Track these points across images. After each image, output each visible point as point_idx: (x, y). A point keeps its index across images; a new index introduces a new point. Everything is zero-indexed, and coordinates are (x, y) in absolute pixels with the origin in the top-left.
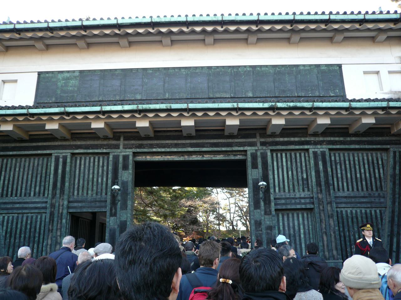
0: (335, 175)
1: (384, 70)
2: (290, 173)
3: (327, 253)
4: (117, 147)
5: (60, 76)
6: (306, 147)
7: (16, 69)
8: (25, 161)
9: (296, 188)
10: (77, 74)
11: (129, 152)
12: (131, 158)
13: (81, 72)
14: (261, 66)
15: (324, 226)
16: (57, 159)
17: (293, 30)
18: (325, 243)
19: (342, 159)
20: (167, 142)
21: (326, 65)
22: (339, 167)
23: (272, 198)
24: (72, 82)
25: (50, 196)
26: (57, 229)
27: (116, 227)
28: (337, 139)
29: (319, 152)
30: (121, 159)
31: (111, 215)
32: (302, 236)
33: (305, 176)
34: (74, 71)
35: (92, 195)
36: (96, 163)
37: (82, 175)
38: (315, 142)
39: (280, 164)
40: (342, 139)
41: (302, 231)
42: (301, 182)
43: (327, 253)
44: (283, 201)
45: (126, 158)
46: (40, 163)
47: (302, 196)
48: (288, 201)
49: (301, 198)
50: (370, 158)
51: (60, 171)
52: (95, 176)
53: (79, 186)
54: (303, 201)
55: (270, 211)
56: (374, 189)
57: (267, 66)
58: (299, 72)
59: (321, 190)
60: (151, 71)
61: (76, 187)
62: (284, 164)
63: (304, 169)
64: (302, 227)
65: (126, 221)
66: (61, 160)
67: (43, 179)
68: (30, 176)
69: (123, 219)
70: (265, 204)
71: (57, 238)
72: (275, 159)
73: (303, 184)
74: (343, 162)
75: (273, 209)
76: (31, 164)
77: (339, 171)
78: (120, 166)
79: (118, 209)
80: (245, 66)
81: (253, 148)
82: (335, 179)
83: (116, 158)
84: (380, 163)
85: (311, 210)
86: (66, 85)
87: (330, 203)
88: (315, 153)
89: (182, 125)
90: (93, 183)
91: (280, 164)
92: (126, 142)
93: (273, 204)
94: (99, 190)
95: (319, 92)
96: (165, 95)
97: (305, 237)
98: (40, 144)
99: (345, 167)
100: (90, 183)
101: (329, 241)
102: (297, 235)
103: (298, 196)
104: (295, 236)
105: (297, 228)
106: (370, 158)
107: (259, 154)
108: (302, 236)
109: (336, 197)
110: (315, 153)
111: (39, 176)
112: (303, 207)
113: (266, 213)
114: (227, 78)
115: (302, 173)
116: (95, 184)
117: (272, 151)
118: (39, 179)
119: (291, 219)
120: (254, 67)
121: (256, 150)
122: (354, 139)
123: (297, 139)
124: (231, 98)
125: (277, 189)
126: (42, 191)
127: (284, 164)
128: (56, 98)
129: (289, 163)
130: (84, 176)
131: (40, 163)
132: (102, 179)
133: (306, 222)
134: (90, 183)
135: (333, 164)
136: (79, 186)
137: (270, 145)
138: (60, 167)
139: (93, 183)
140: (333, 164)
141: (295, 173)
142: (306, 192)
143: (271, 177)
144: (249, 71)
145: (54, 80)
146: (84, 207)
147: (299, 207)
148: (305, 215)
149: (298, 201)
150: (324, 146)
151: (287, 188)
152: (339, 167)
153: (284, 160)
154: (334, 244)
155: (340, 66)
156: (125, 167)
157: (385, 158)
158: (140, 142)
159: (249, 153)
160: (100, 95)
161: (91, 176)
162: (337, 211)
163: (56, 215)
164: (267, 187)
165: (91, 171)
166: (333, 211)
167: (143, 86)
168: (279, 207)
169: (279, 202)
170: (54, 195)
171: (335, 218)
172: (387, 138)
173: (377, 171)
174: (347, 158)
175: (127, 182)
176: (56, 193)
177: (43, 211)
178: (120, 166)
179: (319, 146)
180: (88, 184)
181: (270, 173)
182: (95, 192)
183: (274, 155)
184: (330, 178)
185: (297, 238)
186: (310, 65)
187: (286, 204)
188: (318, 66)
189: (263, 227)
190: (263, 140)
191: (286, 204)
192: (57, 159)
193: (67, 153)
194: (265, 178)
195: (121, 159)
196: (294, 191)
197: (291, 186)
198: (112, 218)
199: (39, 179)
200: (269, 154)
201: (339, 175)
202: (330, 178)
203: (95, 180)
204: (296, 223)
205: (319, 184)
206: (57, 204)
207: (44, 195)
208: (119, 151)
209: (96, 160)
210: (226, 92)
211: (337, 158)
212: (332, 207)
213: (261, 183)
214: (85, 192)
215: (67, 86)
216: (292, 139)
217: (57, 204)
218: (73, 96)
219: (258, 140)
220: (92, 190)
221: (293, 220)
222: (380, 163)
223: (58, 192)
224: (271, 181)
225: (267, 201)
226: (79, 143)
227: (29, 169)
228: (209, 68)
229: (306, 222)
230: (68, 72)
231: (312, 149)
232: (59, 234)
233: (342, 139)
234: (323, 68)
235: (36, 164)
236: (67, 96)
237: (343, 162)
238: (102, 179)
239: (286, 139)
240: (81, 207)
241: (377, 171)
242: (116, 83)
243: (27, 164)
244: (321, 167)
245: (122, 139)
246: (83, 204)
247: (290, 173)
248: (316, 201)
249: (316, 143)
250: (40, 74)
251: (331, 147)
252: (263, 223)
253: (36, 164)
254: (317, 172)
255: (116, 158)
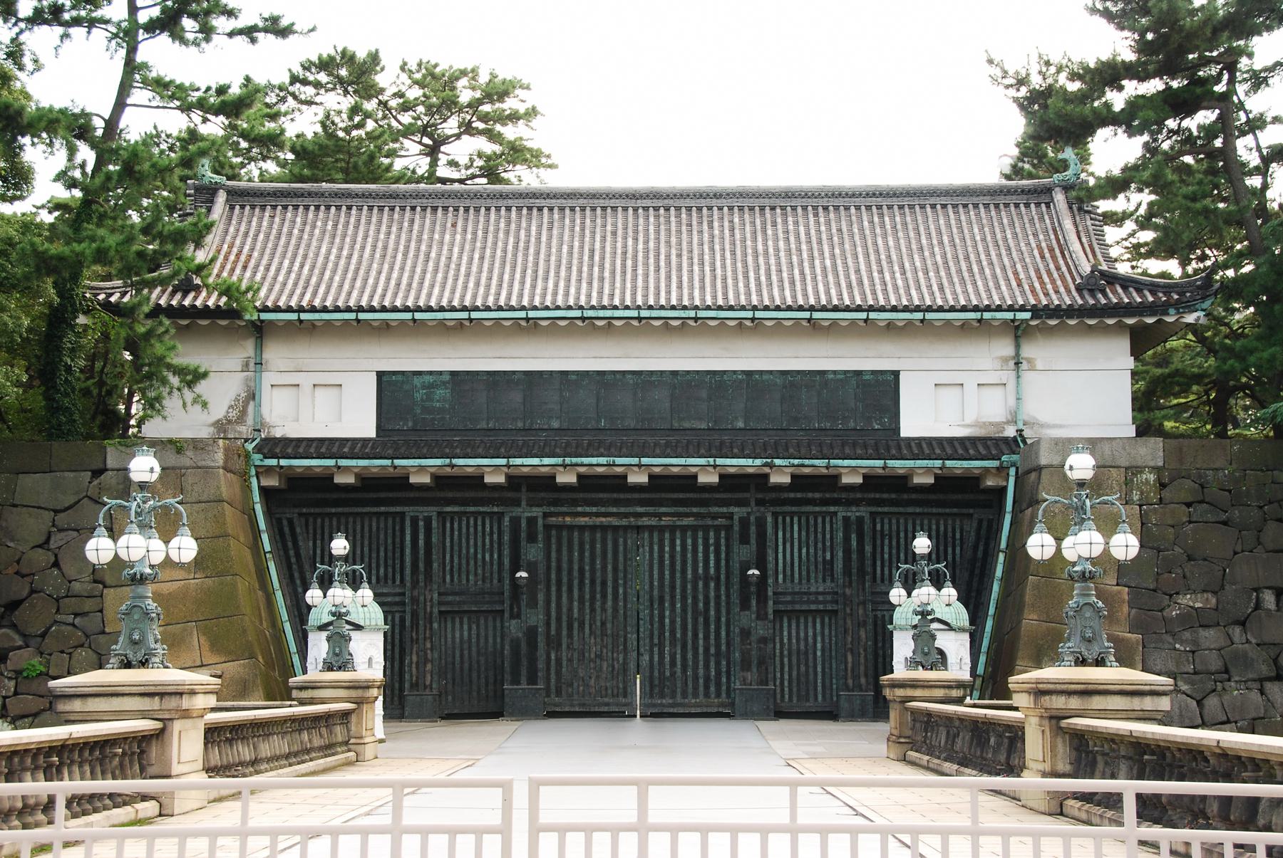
0: (878, 556)
1: (970, 381)
2: (804, 550)
3: (850, 682)
4: (517, 503)
5: (417, 381)
6: (832, 509)
7: (337, 364)
8: (354, 522)
9: (813, 575)
10: (447, 378)
11: (537, 512)
12: (540, 522)
13: (453, 373)
14: (761, 372)
15: (849, 639)
16: (414, 521)
17: (813, 323)
18: (850, 665)
19: (894, 527)
20: (601, 495)
21: (873, 372)
22: (886, 542)
23: (770, 593)
24: (440, 392)
25: (408, 584)
26: (425, 639)
27: (520, 635)
28: (885, 496)
29: (853, 518)
30: (524, 524)
31: (512, 617)
32: (819, 653)
33: (828, 557)
34: (441, 373)
35: (476, 582)
36: (480, 528)
37: (456, 548)
38: (847, 500)
39: (788, 535)
40: (893, 496)
41: (819, 646)
42: (820, 567)
43: (850, 682)
44: (789, 598)
45: (532, 521)
46: (382, 525)
47: (821, 589)
48: (797, 598)
49: (818, 593)
50: (942, 528)
51: (421, 542)
52: (480, 551)
53: (452, 567)
54: (821, 598)
55: (766, 614)
56: (796, 581)
57: (771, 372)
58: (826, 384)
59: (850, 582)
60: (574, 377)
61: (448, 568)
62: (796, 535)
63: (828, 544)
64: (819, 639)
65: (536, 627)
66: (421, 523)
67: (390, 554)
68: (366, 549)
69: (532, 622)
70: (758, 602)
71: (426, 654)
72: (780, 526)
73: (824, 569)
74: (894, 534)
75: (770, 611)
76: (366, 529)
77: (886, 549)
78: (523, 535)
79: (523, 608)
80: (735, 372)
81: (744, 510)
82: (879, 563)
83: (515, 522)
84: (958, 536)
85: (835, 612)
86: (429, 397)
87: (864, 603)
88: (846, 519)
89: (373, 434)
90: (476, 563)
91: (788, 535)
92: (532, 495)
93: (771, 603)
94: (488, 575)
95: (855, 421)
96: (599, 421)
97: (823, 655)
98: (383, 495)
99: (898, 542)
100: (472, 562)
101: (856, 664)
102: (811, 651)
103: (813, 589)
104: (806, 653)
105: (810, 640)
106: (942, 528)
107: (752, 518)
108: (819, 653)
109: (873, 593)
110: (846, 519)
111: (382, 549)
112: (821, 607)
113: (758, 618)
114: (704, 394)
115: (824, 551)
116: (480, 563)
117: (775, 515)
118: (382, 554)
119: (802, 627)
120: (749, 374)
121: (749, 514)
122: (914, 496)
123: (817, 495)
124: (709, 429)
125: (781, 577)
126: (390, 575)
127: (796, 535)
128: (415, 423)
129: (804, 533)
130: (460, 551)
131: (382, 525)
132: (492, 556)
133: (827, 632)
134: (472, 562)
135: (878, 536)
136: (452, 567)
137: (772, 505)
138: (421, 536)
139: (476, 563)
140: (878, 536)
141: (812, 551)
142: (828, 583)
143: (771, 558)
144: (741, 381)
145: (406, 387)
146: (464, 603)
147: (813, 607)
148: (827, 620)
149: (812, 598)
150: (862, 508)
151: (797, 576)
152: (886, 542)
153: (796, 528)
154: (862, 668)
155: (896, 374)
156: (532, 538)
157: (967, 528)
158: (556, 495)
159: (736, 517)
160: (488, 419)
161: (472, 550)
162: (876, 616)
163: (421, 615)
164: (763, 577)
165: (472, 542)
166: (867, 616)
167: (561, 404)
168: (782, 607)
169: (782, 599)
170: (415, 584)
171: (870, 627)
172: (972, 497)
173: (950, 550)
174: (902, 528)
175: (536, 563)
176: (418, 582)
177: (396, 608)
178: (523, 535)
179: (854, 509)
180: (468, 564)
181: (770, 552)
182: (480, 577)
183: (780, 519)
184: (868, 562)
185: (811, 657)
186: (845, 372)
187: (792, 602)
188: (858, 373)
189: (753, 638)
190: (760, 496)
191: (792, 602)
192: (414, 521)
193: (432, 511)
194: (761, 565)
195: (524, 524)
196: (808, 581)
197: (804, 573)
198: (514, 622)
199: (382, 554)
200: (769, 519)
201: (886, 556)
202: (868, 562)
203: (479, 556)
204: (810, 633)
205: (847, 571)
206: (422, 598)
207: (394, 582)
208: (520, 510)
209: (479, 523)
210: (700, 419)
211: (886, 527)
212: (865, 610)
213: (750, 572)
214: (464, 577)
215: (432, 400)
216: (810, 495)
217: (422, 598)
218: (443, 419)
219: (751, 495)
220: (476, 575)
221: (806, 628)
222: (958, 536)
223: (421, 577)
224: (771, 566)
225: (762, 599)
226: (450, 495)
227: (362, 537)
228: (675, 373)
229: (827, 632)
230: (431, 373)
231: (842, 512)
232: (428, 645)
233: (893, 496)
234: (867, 377)
235: (374, 529)
236: (433, 419)
237: (894, 534)
238: (492, 556)
239: (799, 495)
240: (459, 603)
241: (950, 550)
242: (516, 397)
243: (358, 528)
244: (854, 543)
245: (524, 489)
246: (463, 598)
247: (804, 550)
248: (841, 600)
249: (849, 503)
250: (380, 375)
251: (874, 509)
252: (753, 632)
253: (374, 529)
254: (847, 551)
255: (515, 522)
